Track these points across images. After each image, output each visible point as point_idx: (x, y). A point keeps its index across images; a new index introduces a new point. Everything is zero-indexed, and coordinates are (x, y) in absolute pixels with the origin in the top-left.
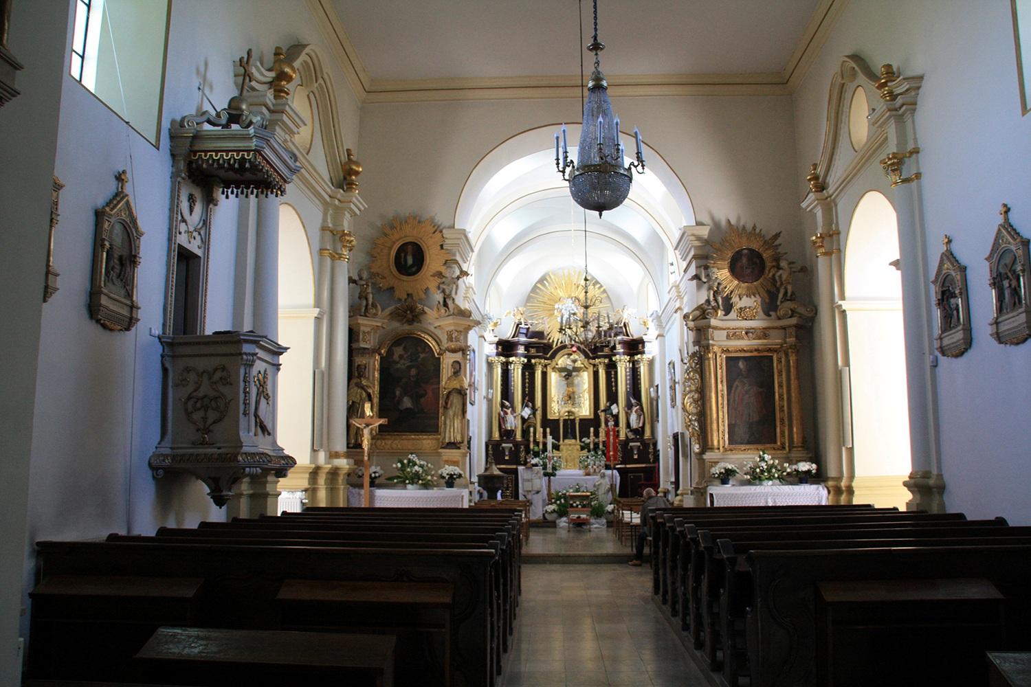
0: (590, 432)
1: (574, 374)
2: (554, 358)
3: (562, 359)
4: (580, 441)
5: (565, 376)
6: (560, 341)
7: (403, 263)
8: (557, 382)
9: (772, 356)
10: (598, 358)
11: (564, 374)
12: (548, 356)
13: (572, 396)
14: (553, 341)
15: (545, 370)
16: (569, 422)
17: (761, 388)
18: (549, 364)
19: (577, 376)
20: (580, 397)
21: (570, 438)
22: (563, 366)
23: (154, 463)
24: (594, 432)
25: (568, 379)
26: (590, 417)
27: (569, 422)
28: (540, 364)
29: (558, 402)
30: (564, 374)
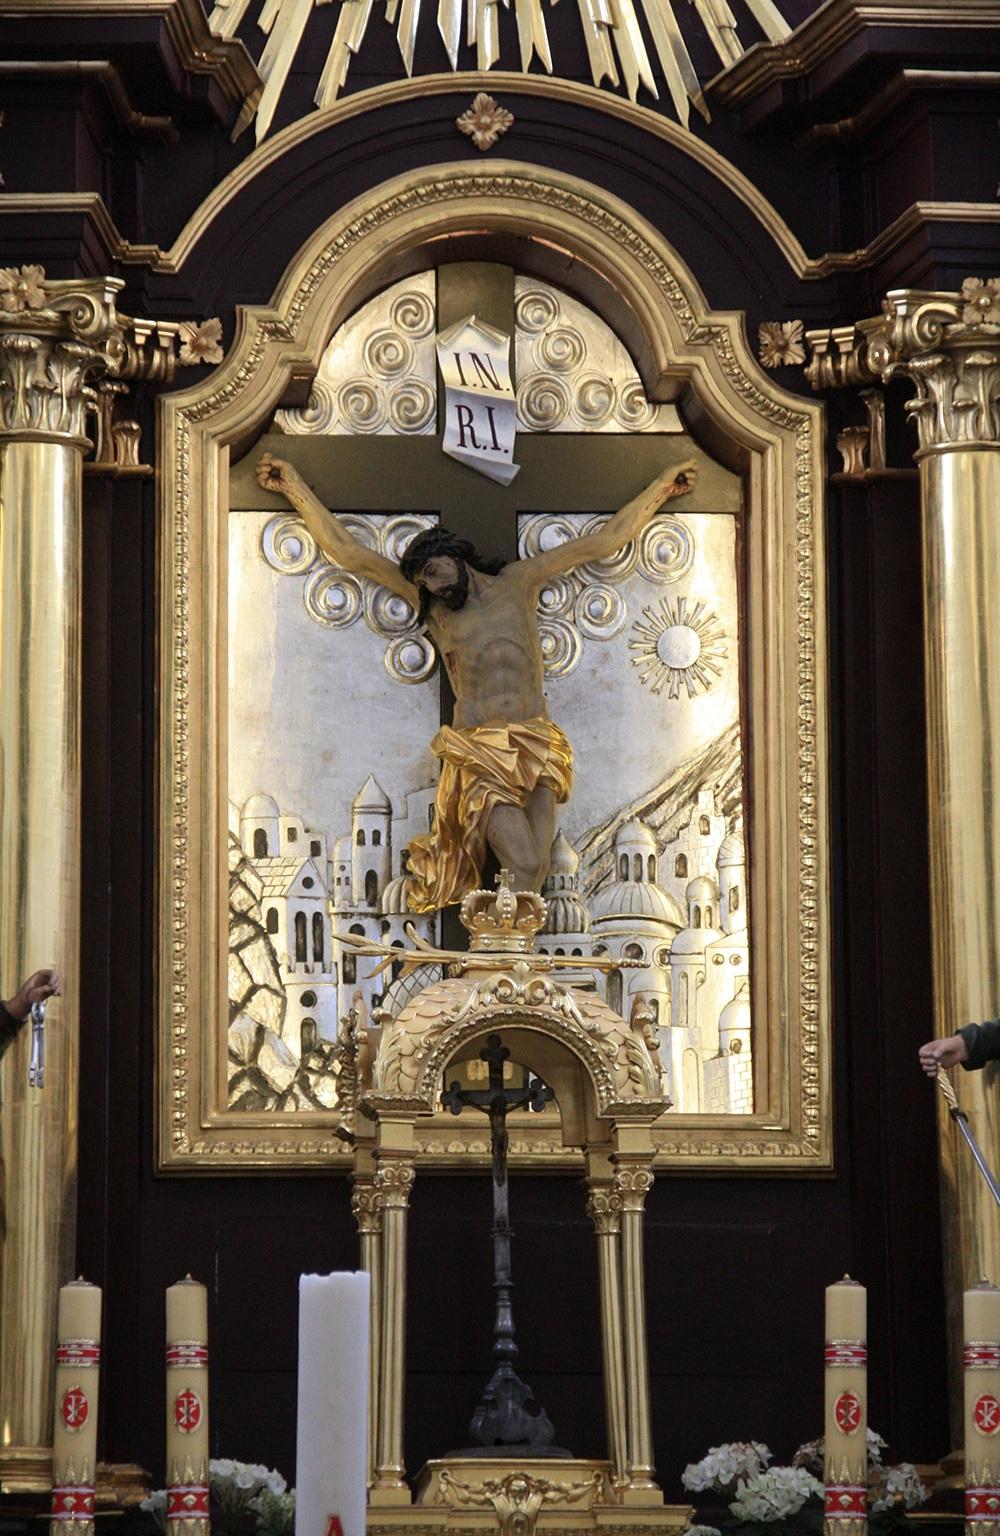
0: (816, 1353)
1: (544, 533)
2: (265, 291)
3: (377, 316)
4: (667, 1475)
5: (413, 563)
6: (351, 32)
7: (122, 1513)
8: (290, 647)
9: (215, 1452)
10: (922, 282)
11: (389, 538)
12: (177, 256)
13: (511, 830)
14: (252, 34)
15: (128, 456)
16: (501, 1195)
17: (539, 1412)
18: (193, 375)
19: (591, 564)
20: (629, 869)
21: (500, 1444)
22: (388, 424)
23: (264, 1490)
24: (877, 1353)
25: (457, 598)
26: (773, 1156)
27: (501, 1195)
28: (58, 340)
29: (309, 934)
30: (389, 538)
